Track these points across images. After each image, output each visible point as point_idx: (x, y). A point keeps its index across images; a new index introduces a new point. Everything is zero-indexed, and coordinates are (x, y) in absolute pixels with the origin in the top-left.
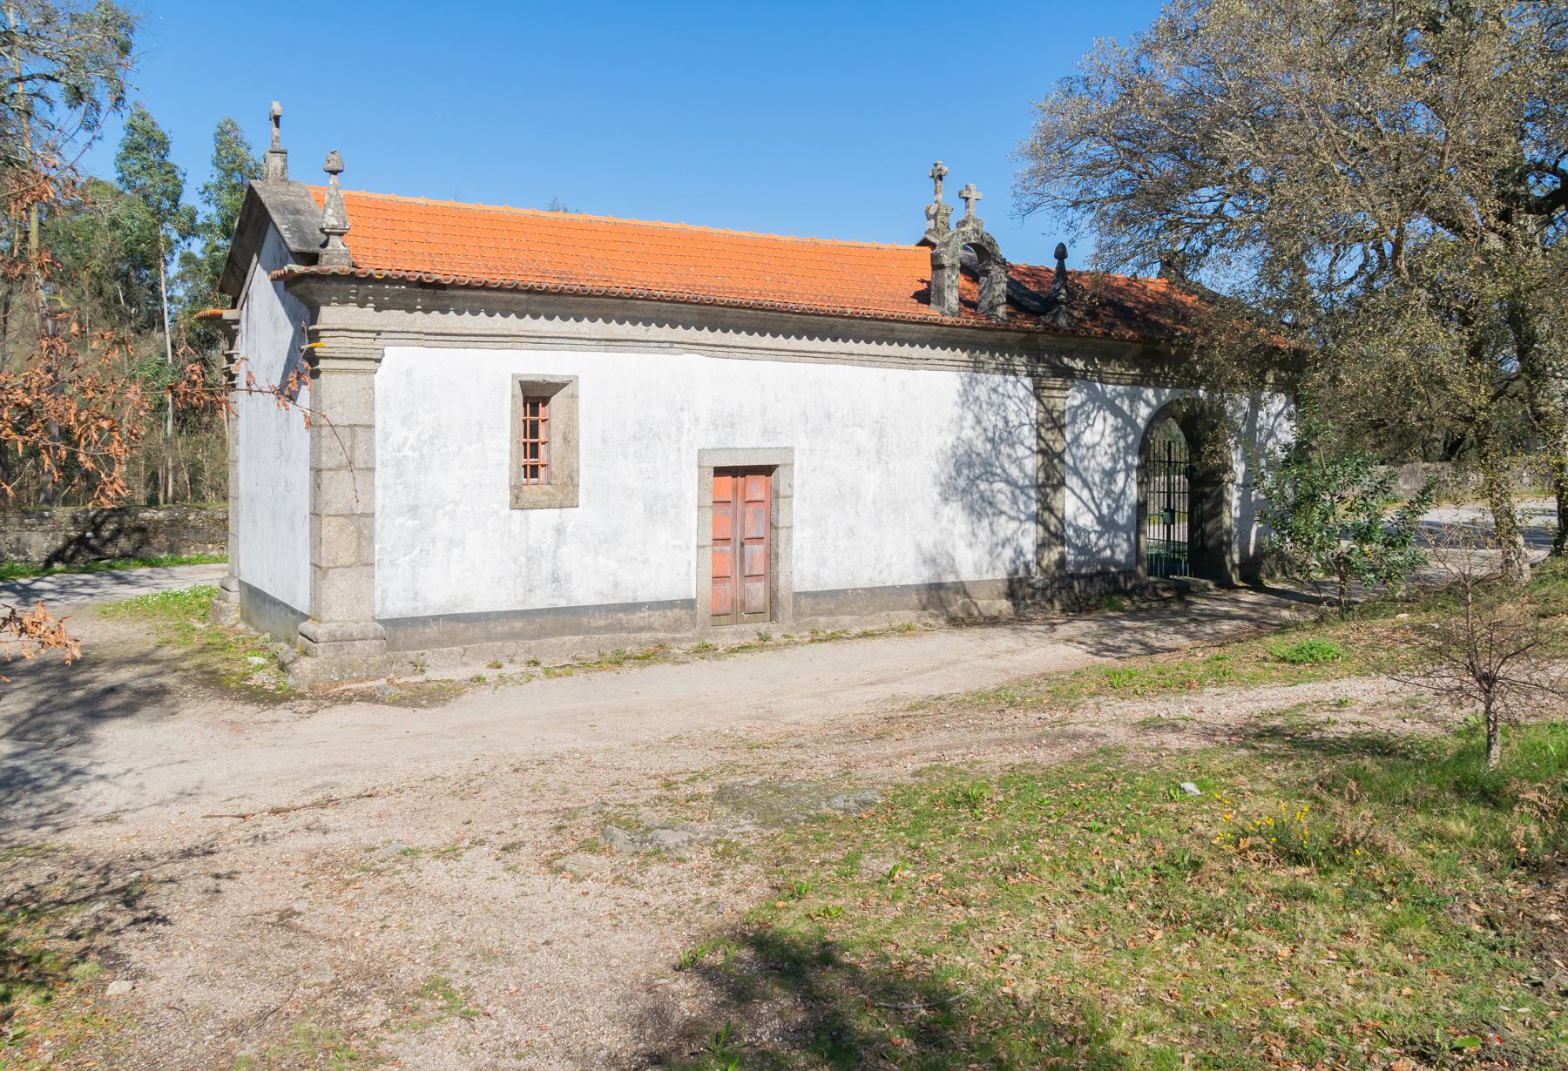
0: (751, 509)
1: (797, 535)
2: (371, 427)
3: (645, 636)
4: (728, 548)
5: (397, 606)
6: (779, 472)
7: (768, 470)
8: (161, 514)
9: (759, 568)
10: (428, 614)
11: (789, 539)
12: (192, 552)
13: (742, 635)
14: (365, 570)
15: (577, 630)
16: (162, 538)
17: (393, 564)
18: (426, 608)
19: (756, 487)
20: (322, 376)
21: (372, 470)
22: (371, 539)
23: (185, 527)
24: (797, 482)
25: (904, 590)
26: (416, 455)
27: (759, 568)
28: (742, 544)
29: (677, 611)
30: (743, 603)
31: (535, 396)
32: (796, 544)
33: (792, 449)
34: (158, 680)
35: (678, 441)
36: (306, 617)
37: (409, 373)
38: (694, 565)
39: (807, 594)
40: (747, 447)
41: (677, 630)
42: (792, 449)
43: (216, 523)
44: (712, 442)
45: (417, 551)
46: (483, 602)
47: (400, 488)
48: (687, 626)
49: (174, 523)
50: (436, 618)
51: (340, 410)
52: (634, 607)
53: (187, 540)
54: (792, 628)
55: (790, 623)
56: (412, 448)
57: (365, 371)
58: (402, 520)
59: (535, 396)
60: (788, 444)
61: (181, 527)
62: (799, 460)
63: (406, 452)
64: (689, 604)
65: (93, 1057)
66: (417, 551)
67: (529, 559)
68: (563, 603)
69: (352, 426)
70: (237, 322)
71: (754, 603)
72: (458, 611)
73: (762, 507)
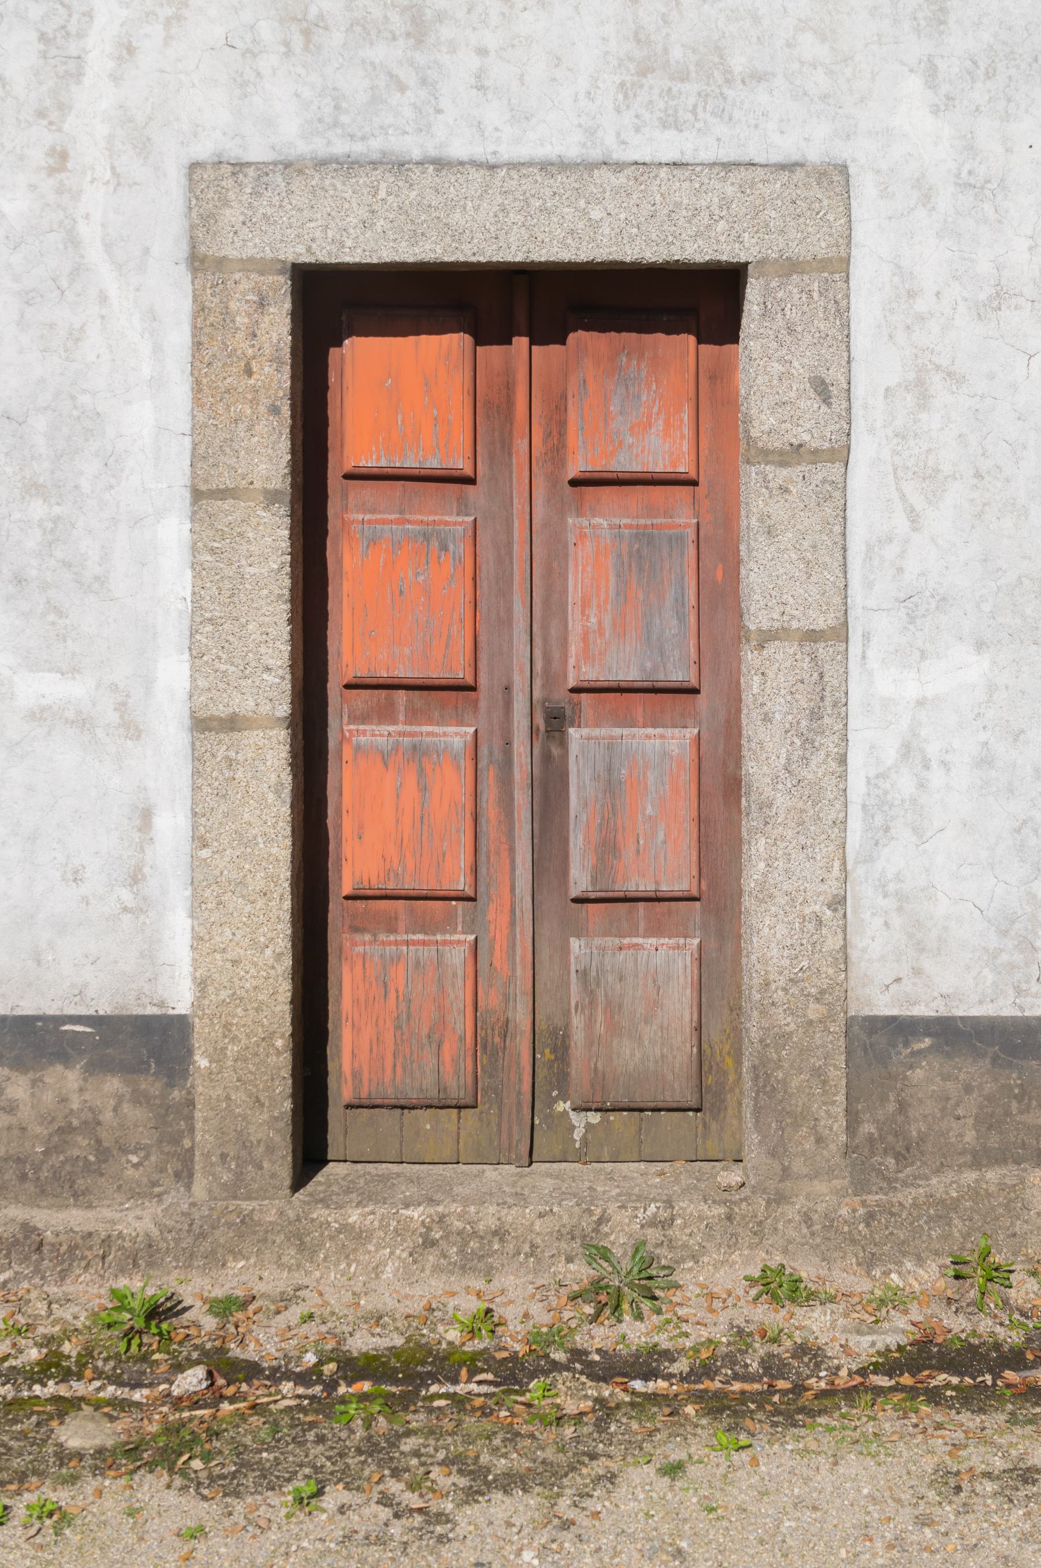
0: (606, 520)
1: (881, 684)
2: (838, 266)
4: (454, 736)
7: (700, 301)
9: (662, 859)
11: (825, 711)
13: (478, 1252)
19: (626, 400)
24: (876, 368)
27: (662, 859)
28: (555, 723)
29: (67, 1079)
30: (552, 1045)
32: (870, 743)
33: (836, 177)
35: (52, 111)
38: (173, 824)
39: (952, 1034)
40: (530, 136)
41: (68, 1184)
42: (836, 177)
44: (281, 120)
48: (131, 1167)
54: (828, 1235)
55: (827, 1194)
60: (810, 140)
62: (877, 244)
64: (148, 1045)
65: (2, 1450)
71: (628, 1055)
73: (680, 512)
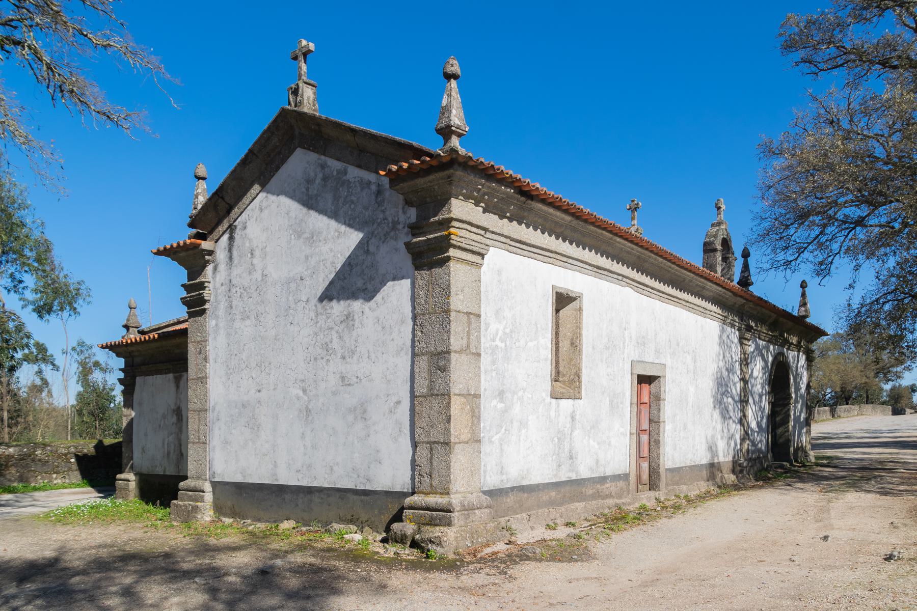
2: (479, 316)
3: (611, 502)
5: (492, 480)
6: (661, 379)
8: (11, 450)
10: (508, 486)
12: (40, 481)
14: (476, 445)
15: (582, 498)
16: (13, 470)
17: (491, 442)
18: (508, 480)
20: (452, 264)
21: (479, 355)
22: (479, 418)
23: (33, 460)
25: (693, 468)
26: (503, 345)
31: (563, 300)
34: (333, 563)
36: (405, 495)
37: (499, 272)
43: (59, 457)
45: (503, 430)
46: (536, 478)
47: (494, 374)
48: (625, 493)
49: (22, 458)
50: (512, 489)
51: (461, 297)
52: (603, 479)
53: (35, 471)
56: (502, 340)
57: (472, 263)
58: (494, 402)
59: (563, 300)
61: (29, 461)
63: (498, 343)
64: (626, 477)
66: (503, 430)
67: (559, 439)
68: (574, 477)
69: (468, 314)
70: (211, 253)
72: (524, 483)
